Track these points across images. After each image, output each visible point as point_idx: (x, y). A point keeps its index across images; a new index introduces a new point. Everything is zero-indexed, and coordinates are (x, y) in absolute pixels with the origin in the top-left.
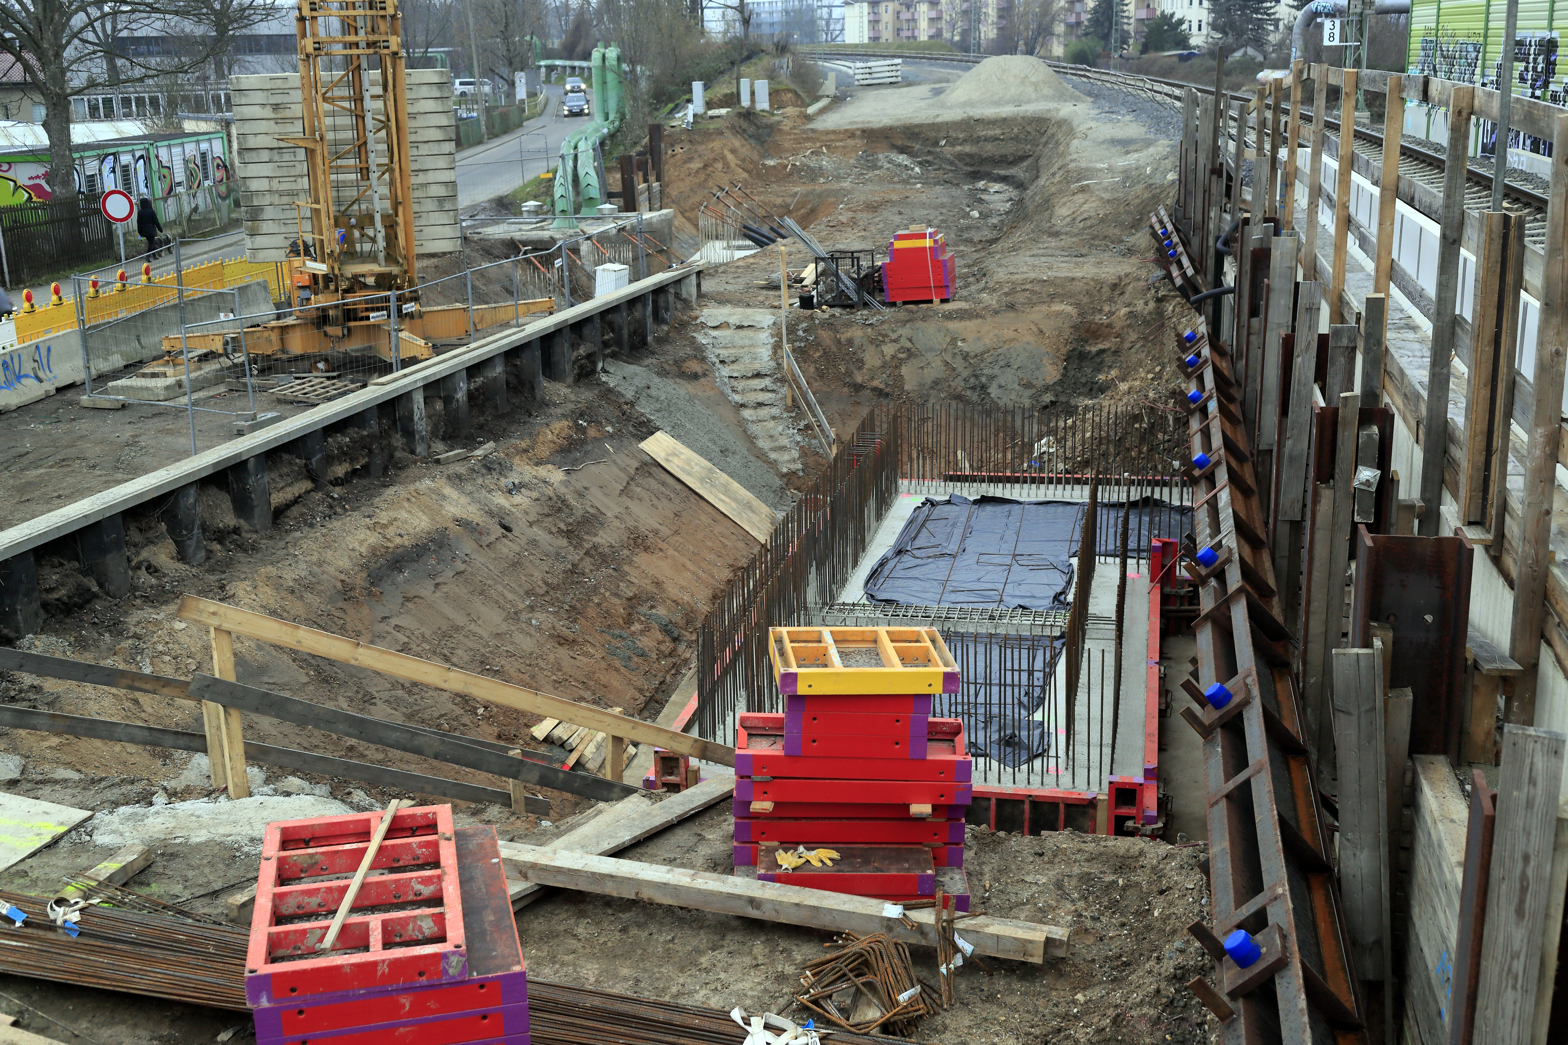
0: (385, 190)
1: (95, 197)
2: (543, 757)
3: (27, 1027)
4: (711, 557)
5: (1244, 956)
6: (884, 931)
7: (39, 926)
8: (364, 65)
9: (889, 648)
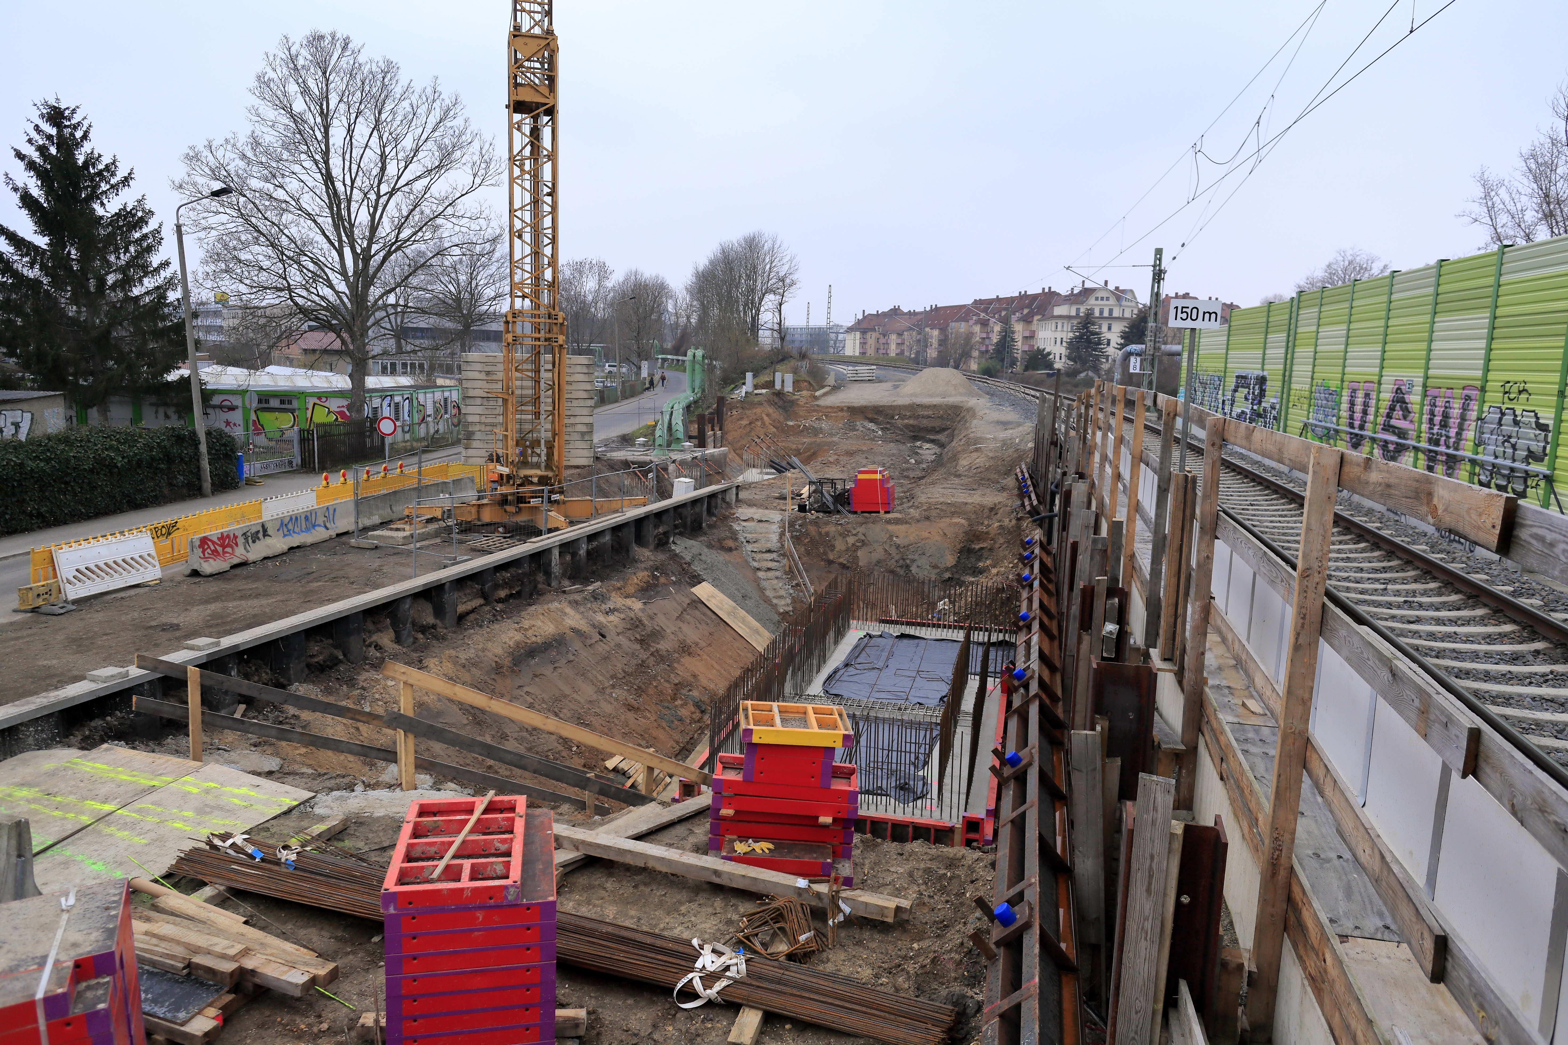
0: (549, 426)
1: (375, 420)
2: (609, 780)
3: (254, 926)
4: (730, 661)
5: (1006, 919)
6: (796, 896)
7: (270, 862)
8: (542, 351)
9: (812, 717)
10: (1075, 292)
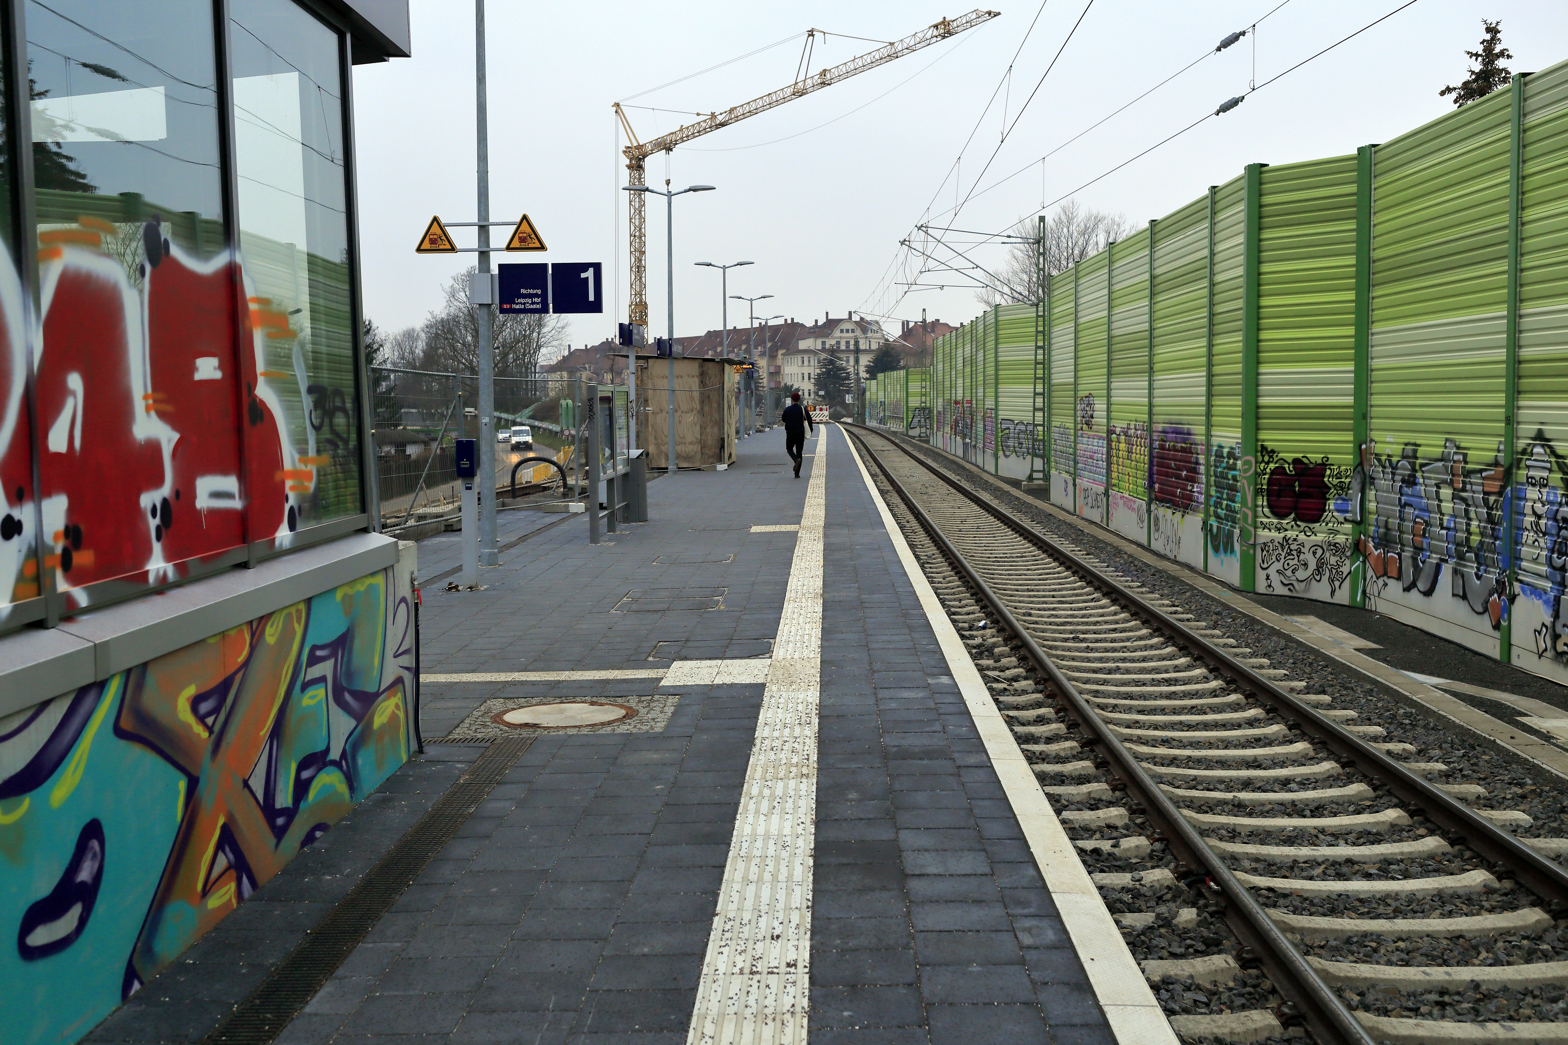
10: (820, 324)
